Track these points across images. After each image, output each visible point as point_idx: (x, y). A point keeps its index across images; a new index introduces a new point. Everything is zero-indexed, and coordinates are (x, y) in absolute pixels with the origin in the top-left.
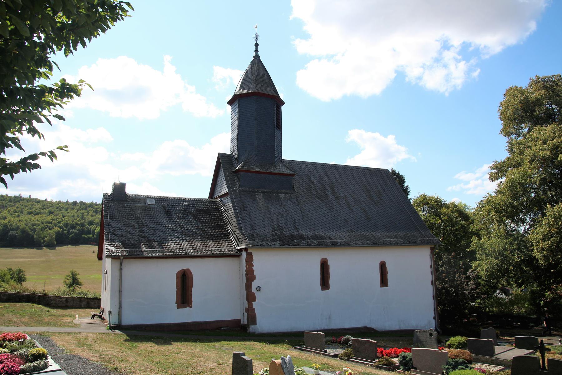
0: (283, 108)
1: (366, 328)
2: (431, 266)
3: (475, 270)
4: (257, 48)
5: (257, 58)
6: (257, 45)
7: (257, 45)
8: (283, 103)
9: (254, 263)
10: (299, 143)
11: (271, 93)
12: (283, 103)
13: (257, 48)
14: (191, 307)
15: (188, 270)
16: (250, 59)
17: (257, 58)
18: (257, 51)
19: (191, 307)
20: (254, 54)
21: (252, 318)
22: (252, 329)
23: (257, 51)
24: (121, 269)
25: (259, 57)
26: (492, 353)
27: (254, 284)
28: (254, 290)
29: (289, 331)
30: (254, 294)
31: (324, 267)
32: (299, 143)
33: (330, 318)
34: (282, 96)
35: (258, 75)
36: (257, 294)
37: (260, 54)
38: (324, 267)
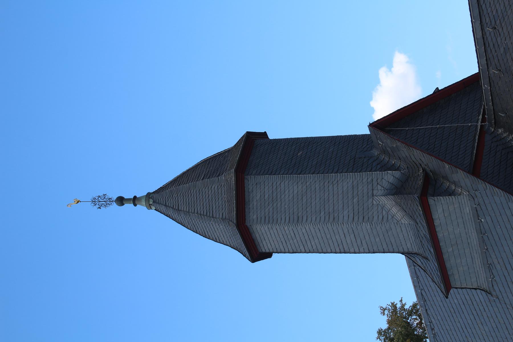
6: (121, 201)
7: (121, 201)
18: (135, 201)
20: (141, 208)
23: (135, 201)
37: (141, 193)
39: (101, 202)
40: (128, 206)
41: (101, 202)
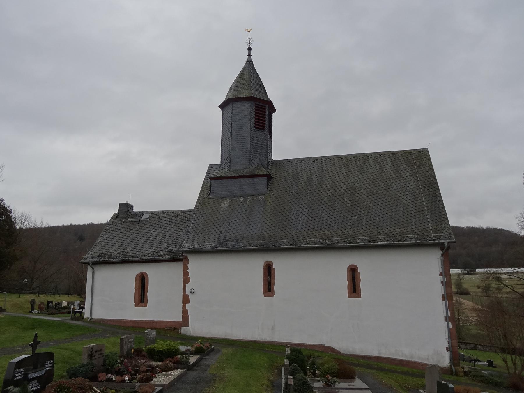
0: (274, 115)
1: (323, 346)
2: (441, 274)
3: (24, 222)
4: (249, 53)
5: (250, 63)
6: (250, 49)
7: (250, 49)
8: (275, 111)
9: (189, 266)
10: (287, 143)
11: (259, 95)
12: (275, 111)
13: (249, 53)
14: (146, 306)
15: (145, 273)
16: (242, 64)
17: (250, 63)
18: (249, 55)
19: (146, 306)
20: (246, 58)
21: (185, 321)
22: (184, 330)
23: (249, 55)
26: (158, 333)
27: (189, 287)
28: (188, 292)
29: (223, 337)
30: (188, 296)
31: (353, 271)
32: (287, 143)
33: (273, 328)
34: (272, 95)
35: (249, 75)
36: (191, 297)
37: (253, 58)
38: (353, 271)
40: (247, 53)
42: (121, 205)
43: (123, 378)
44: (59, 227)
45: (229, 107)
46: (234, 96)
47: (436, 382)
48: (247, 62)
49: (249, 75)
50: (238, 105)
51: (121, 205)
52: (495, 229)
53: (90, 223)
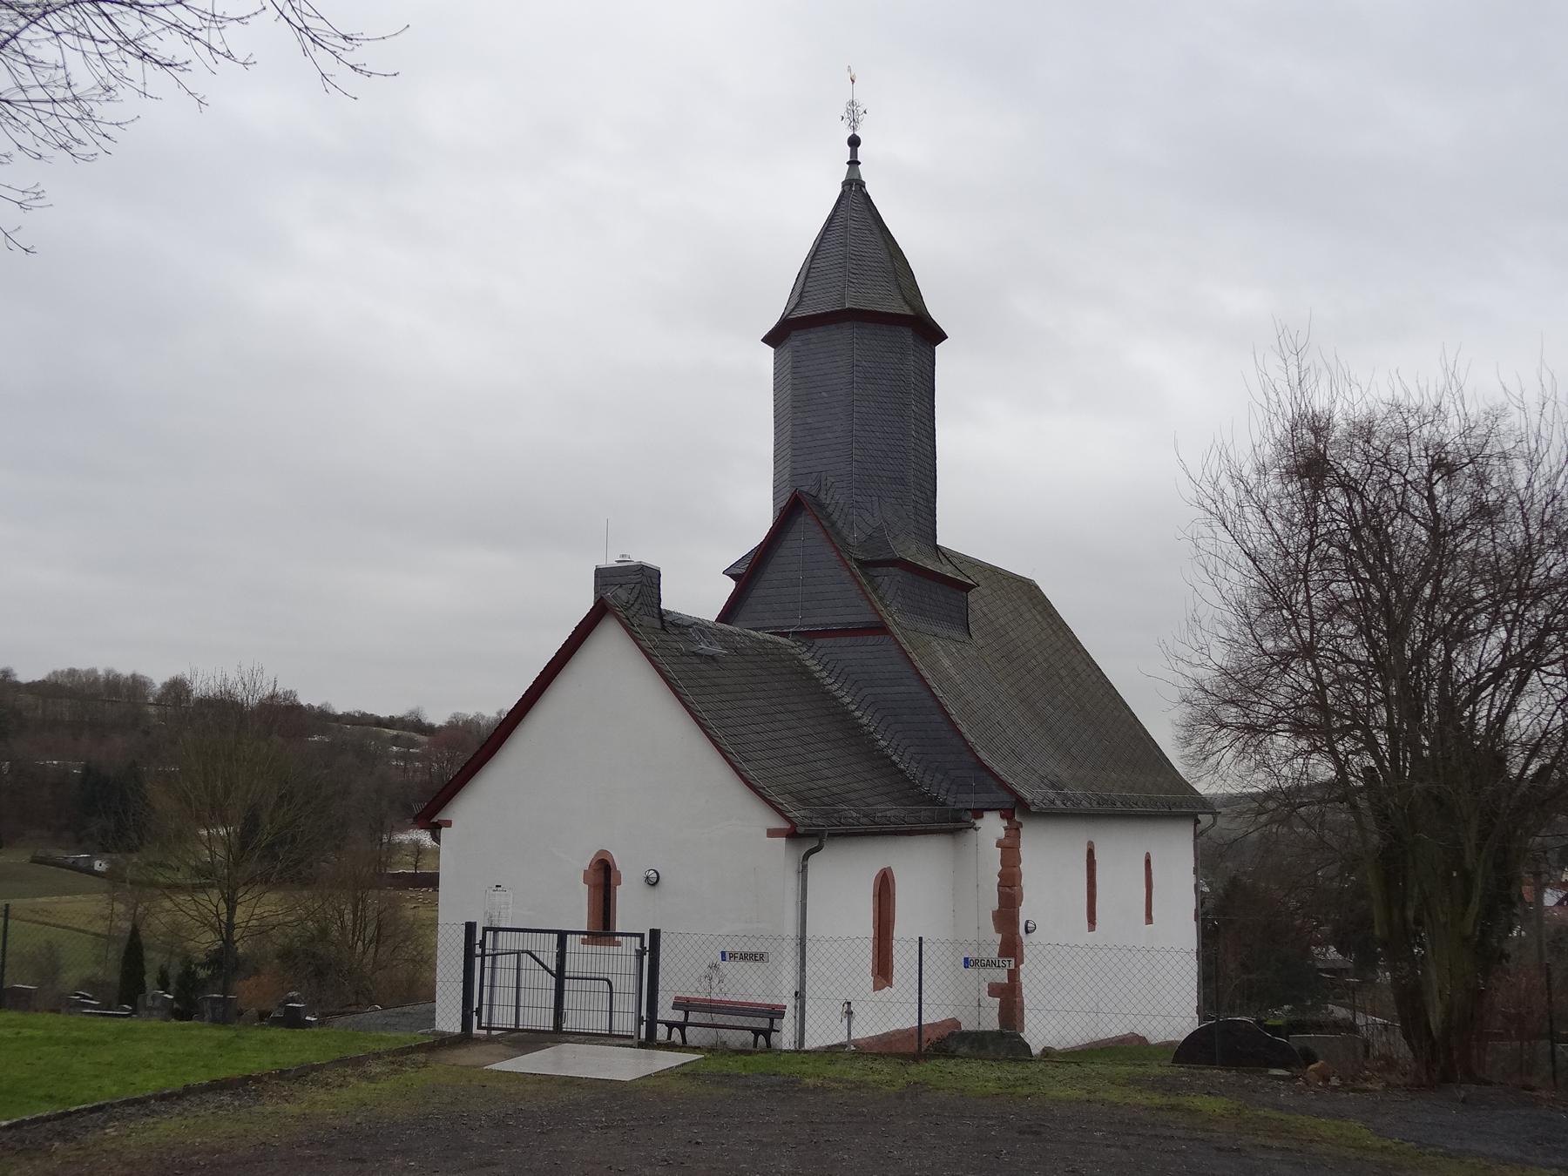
4: (854, 153)
5: (854, 189)
6: (854, 142)
7: (854, 142)
8: (941, 336)
9: (1025, 850)
10: (697, 591)
11: (898, 307)
12: (941, 336)
13: (854, 153)
17: (854, 189)
18: (854, 163)
20: (842, 172)
23: (854, 163)
24: (803, 871)
25: (862, 185)
31: (884, 888)
35: (855, 222)
37: (865, 172)
39: (853, 114)
41: (853, 114)
42: (604, 577)
43: (172, 987)
44: (415, 725)
45: (796, 340)
46: (797, 314)
47: (880, 993)
48: (844, 184)
49: (855, 222)
50: (841, 336)
51: (604, 577)
52: (284, 718)
53: (125, 670)
